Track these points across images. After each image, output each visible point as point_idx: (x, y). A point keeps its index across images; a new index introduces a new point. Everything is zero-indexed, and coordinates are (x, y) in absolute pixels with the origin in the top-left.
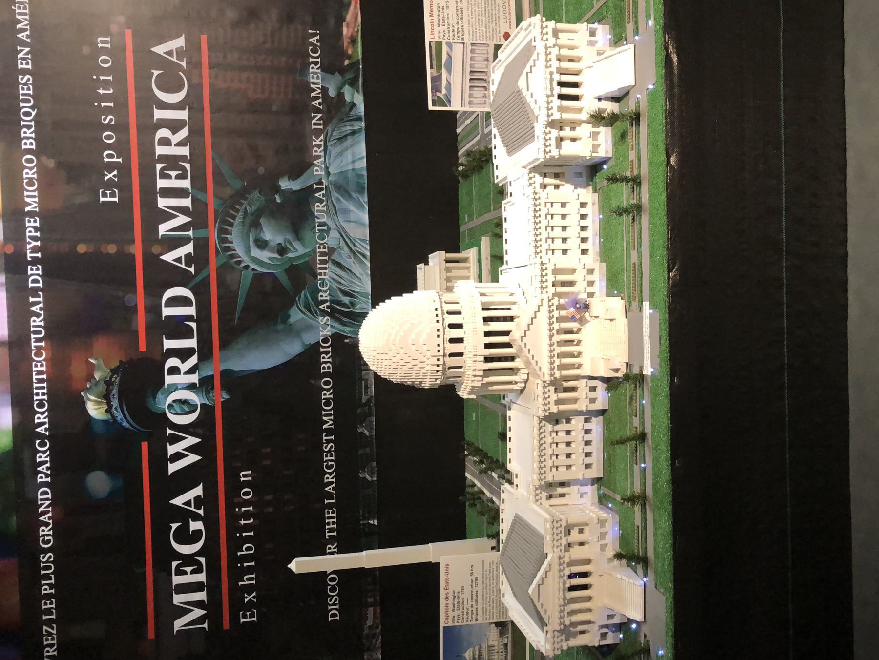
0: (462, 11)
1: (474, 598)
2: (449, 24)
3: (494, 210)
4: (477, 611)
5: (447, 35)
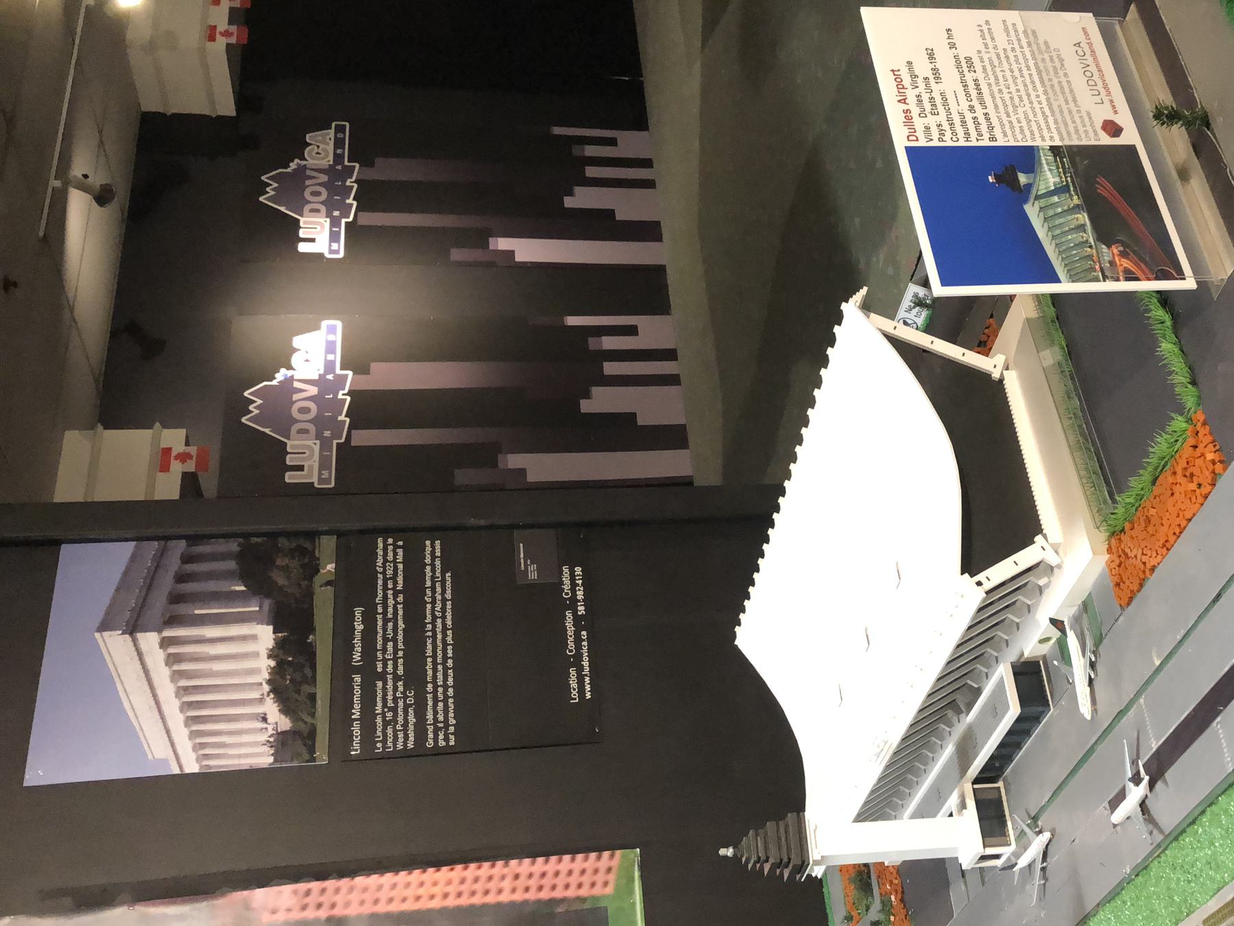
1: (974, 93)
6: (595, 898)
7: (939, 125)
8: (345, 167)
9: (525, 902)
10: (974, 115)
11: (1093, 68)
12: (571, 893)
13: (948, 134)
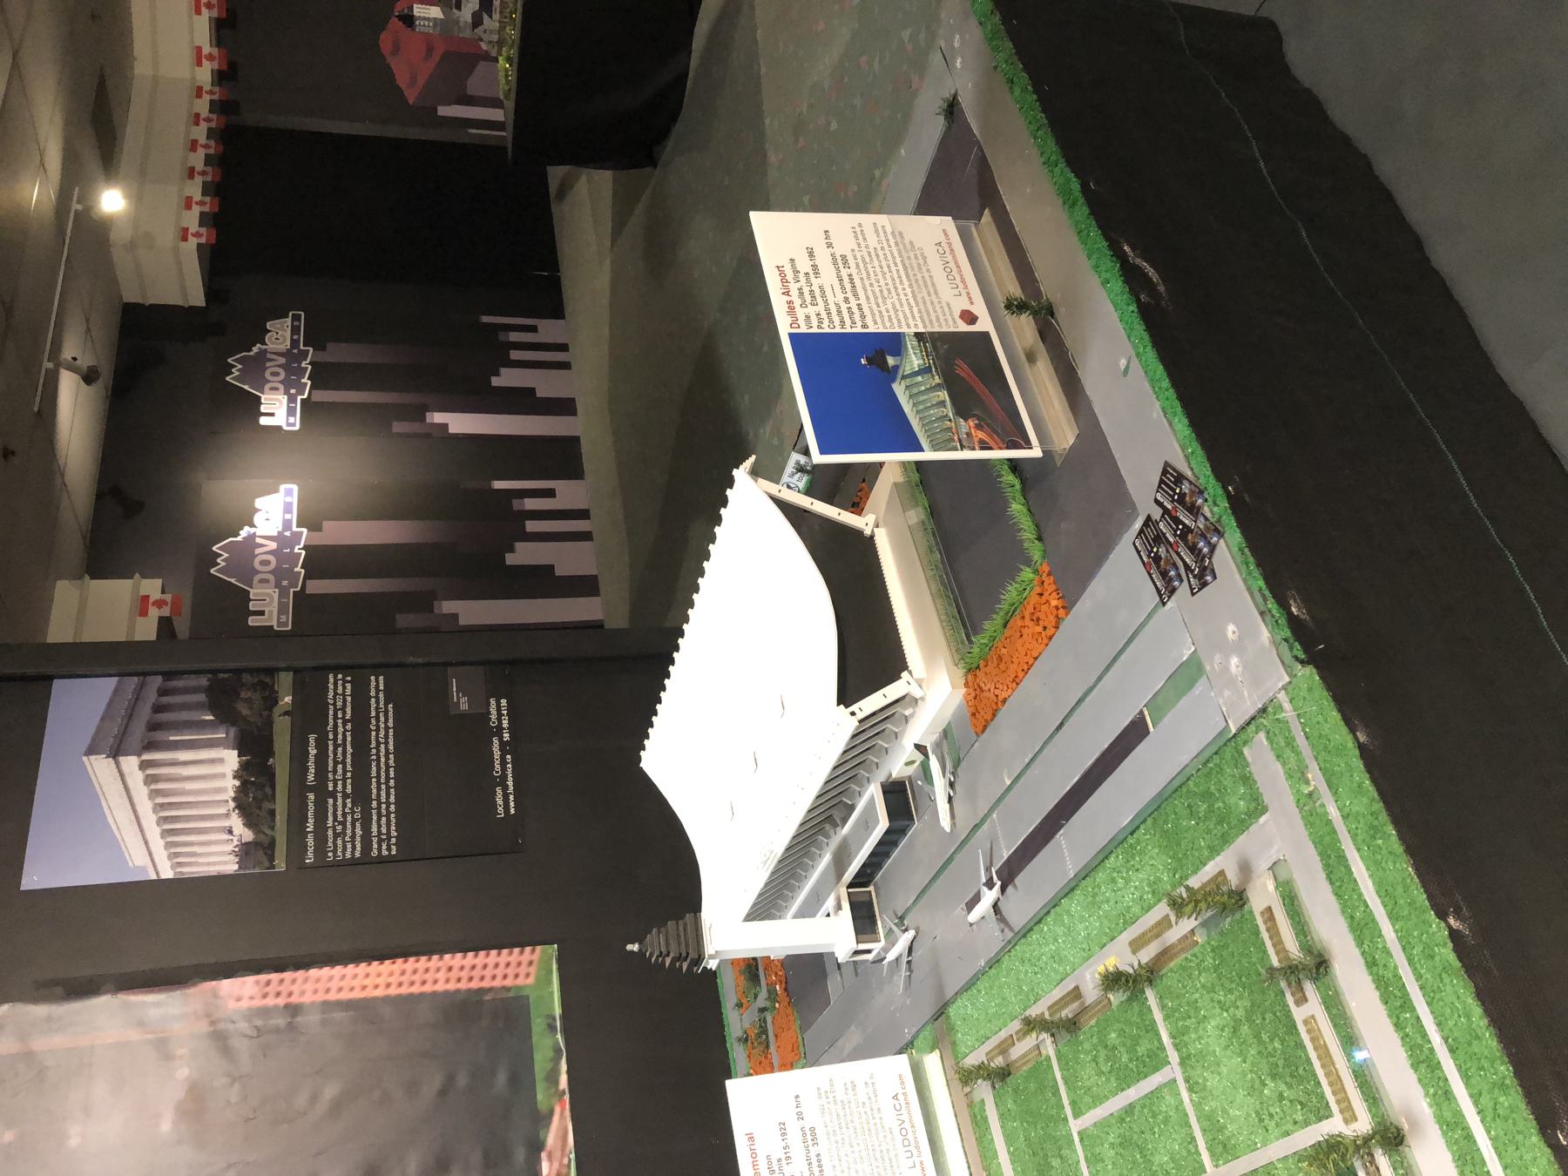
0: (819, 1161)
1: (848, 286)
3: (1012, 1035)
6: (518, 988)
7: (818, 314)
8: (300, 351)
9: (458, 991)
10: (848, 306)
12: (498, 983)
13: (826, 322)
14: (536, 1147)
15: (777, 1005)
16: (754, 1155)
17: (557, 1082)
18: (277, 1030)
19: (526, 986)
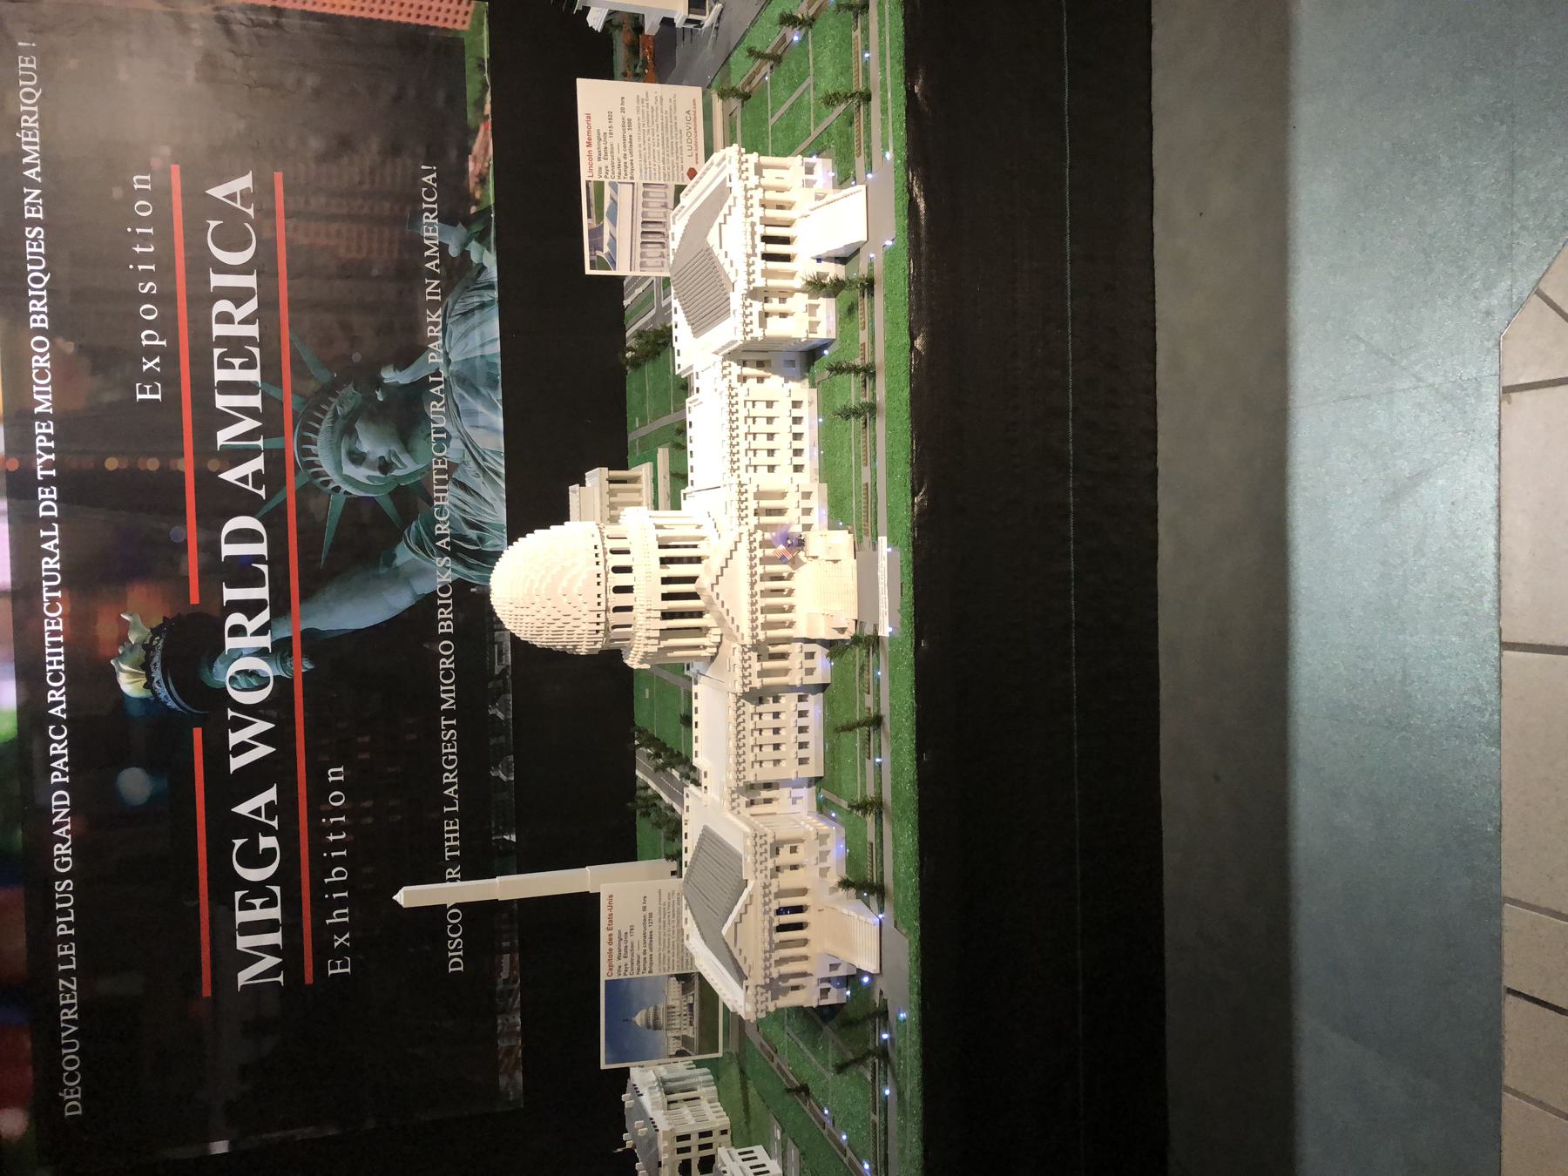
0: (651, 935)
2: (613, 157)
4: (632, 164)
5: (629, 970)
6: (456, 31)
9: (408, 24)
11: (692, 130)
12: (440, 24)
14: (465, 151)
15: (646, 71)
16: (589, 127)
17: (482, 108)
18: (265, 25)
19: (463, 31)
